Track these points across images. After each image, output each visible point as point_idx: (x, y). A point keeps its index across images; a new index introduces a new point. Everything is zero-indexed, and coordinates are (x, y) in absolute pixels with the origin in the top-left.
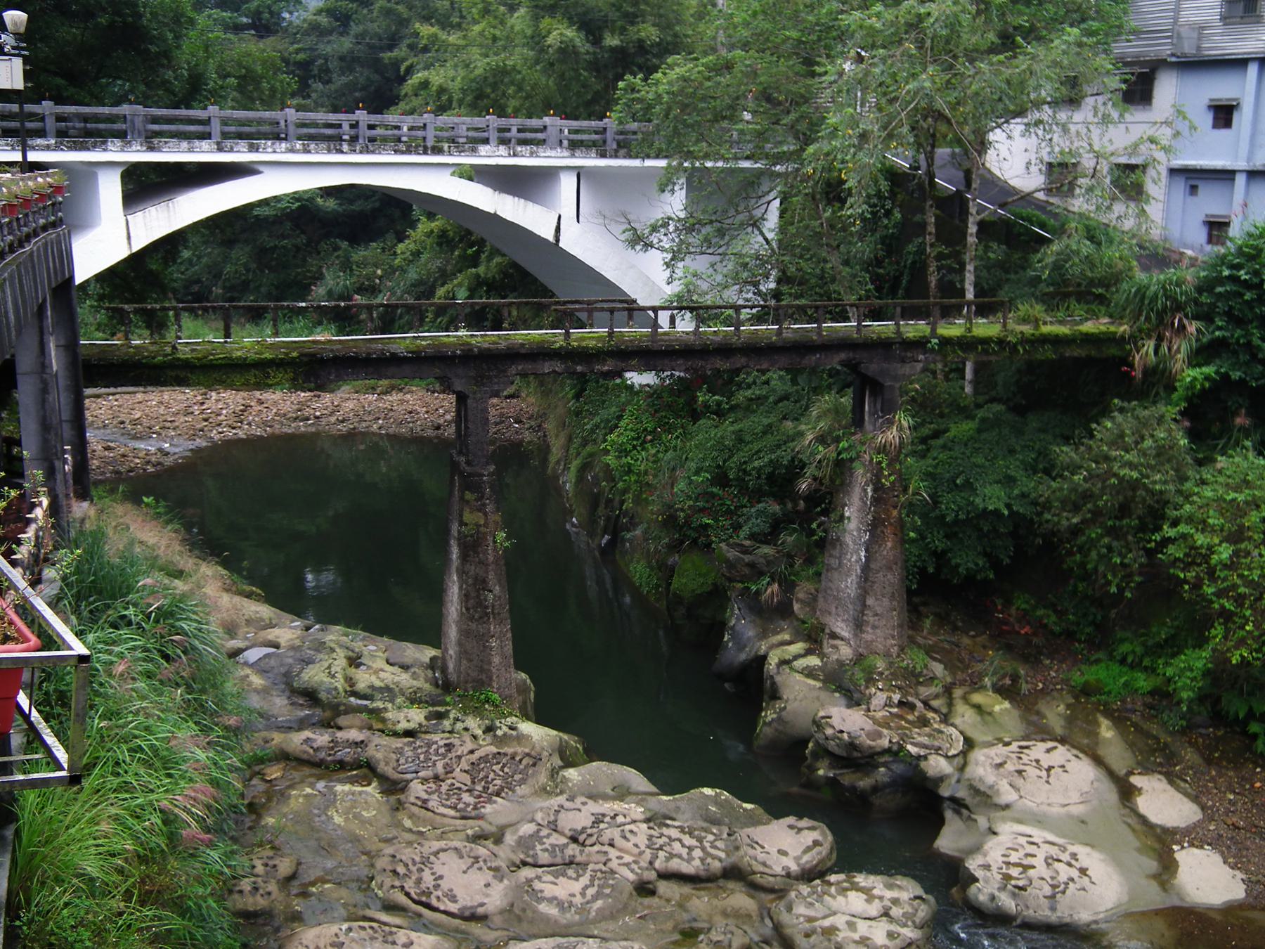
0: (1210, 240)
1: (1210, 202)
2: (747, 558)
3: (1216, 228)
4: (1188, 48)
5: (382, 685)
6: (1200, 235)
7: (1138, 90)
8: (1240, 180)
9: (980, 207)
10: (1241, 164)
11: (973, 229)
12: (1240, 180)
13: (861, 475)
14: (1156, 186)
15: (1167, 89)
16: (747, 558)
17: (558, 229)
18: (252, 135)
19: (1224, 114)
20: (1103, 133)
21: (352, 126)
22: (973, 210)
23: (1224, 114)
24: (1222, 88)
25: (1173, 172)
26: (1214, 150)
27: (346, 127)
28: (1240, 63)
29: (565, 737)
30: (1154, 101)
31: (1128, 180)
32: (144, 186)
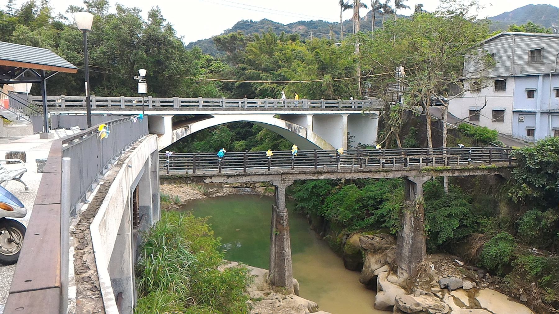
0: (529, 135)
1: (528, 122)
2: (370, 242)
3: (531, 132)
4: (518, 72)
5: (453, 293)
6: (526, 133)
7: (500, 85)
8: (538, 115)
9: (447, 125)
10: (538, 110)
11: (445, 132)
12: (538, 115)
13: (408, 214)
14: (508, 116)
15: (510, 85)
16: (370, 242)
17: (307, 134)
18: (214, 108)
19: (531, 93)
20: (490, 99)
21: (242, 103)
22: (445, 126)
23: (531, 93)
24: (530, 84)
25: (514, 112)
26: (528, 105)
27: (240, 103)
28: (537, 76)
29: (310, 302)
30: (480, 120)
31: (498, 115)
32: (178, 122)
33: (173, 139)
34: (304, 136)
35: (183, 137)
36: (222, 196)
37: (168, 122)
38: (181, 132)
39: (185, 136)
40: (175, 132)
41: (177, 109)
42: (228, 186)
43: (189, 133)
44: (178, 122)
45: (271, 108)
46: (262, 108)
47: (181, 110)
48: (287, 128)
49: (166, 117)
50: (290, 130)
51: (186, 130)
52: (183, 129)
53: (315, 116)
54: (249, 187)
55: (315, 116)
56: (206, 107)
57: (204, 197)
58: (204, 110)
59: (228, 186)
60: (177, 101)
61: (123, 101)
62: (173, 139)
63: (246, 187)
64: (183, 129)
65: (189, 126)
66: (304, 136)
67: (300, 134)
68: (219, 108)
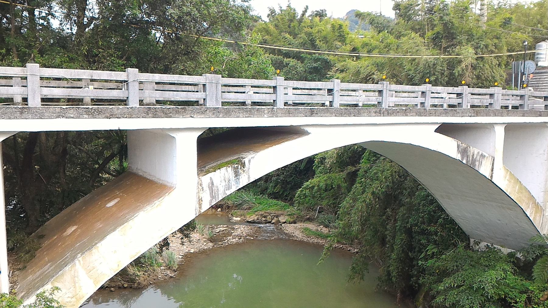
18: (312, 109)
32: (216, 146)
33: (200, 201)
34: (488, 176)
35: (228, 193)
36: (238, 244)
37: (186, 147)
38: (225, 181)
39: (234, 189)
40: (206, 179)
41: (216, 112)
42: (239, 219)
43: (244, 181)
44: (216, 146)
45: (421, 110)
46: (404, 110)
47: (227, 114)
48: (458, 157)
49: (179, 136)
50: (464, 161)
51: (237, 174)
52: (230, 169)
53: (509, 128)
54: (270, 222)
55: (509, 128)
56: (149, 109)
57: (211, 245)
58: (289, 114)
59: (239, 219)
60: (212, 87)
61: (34, 83)
62: (200, 201)
63: (267, 222)
64: (230, 169)
65: (246, 160)
66: (487, 174)
67: (481, 171)
68: (325, 109)
